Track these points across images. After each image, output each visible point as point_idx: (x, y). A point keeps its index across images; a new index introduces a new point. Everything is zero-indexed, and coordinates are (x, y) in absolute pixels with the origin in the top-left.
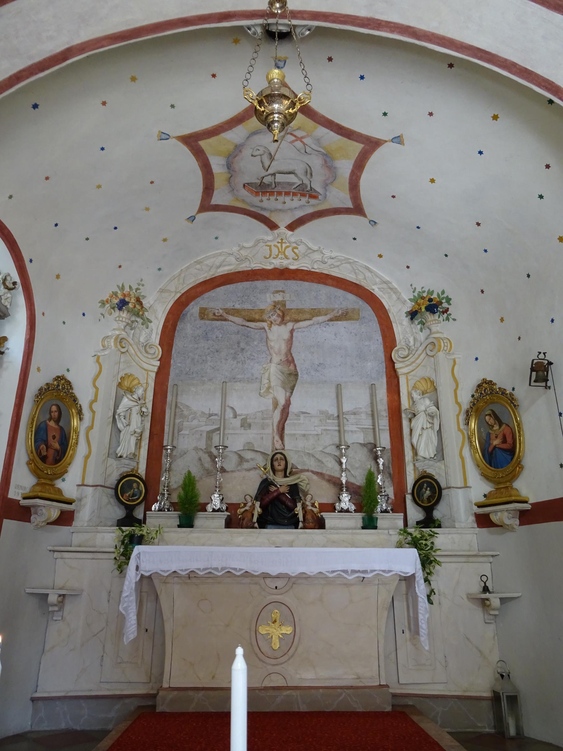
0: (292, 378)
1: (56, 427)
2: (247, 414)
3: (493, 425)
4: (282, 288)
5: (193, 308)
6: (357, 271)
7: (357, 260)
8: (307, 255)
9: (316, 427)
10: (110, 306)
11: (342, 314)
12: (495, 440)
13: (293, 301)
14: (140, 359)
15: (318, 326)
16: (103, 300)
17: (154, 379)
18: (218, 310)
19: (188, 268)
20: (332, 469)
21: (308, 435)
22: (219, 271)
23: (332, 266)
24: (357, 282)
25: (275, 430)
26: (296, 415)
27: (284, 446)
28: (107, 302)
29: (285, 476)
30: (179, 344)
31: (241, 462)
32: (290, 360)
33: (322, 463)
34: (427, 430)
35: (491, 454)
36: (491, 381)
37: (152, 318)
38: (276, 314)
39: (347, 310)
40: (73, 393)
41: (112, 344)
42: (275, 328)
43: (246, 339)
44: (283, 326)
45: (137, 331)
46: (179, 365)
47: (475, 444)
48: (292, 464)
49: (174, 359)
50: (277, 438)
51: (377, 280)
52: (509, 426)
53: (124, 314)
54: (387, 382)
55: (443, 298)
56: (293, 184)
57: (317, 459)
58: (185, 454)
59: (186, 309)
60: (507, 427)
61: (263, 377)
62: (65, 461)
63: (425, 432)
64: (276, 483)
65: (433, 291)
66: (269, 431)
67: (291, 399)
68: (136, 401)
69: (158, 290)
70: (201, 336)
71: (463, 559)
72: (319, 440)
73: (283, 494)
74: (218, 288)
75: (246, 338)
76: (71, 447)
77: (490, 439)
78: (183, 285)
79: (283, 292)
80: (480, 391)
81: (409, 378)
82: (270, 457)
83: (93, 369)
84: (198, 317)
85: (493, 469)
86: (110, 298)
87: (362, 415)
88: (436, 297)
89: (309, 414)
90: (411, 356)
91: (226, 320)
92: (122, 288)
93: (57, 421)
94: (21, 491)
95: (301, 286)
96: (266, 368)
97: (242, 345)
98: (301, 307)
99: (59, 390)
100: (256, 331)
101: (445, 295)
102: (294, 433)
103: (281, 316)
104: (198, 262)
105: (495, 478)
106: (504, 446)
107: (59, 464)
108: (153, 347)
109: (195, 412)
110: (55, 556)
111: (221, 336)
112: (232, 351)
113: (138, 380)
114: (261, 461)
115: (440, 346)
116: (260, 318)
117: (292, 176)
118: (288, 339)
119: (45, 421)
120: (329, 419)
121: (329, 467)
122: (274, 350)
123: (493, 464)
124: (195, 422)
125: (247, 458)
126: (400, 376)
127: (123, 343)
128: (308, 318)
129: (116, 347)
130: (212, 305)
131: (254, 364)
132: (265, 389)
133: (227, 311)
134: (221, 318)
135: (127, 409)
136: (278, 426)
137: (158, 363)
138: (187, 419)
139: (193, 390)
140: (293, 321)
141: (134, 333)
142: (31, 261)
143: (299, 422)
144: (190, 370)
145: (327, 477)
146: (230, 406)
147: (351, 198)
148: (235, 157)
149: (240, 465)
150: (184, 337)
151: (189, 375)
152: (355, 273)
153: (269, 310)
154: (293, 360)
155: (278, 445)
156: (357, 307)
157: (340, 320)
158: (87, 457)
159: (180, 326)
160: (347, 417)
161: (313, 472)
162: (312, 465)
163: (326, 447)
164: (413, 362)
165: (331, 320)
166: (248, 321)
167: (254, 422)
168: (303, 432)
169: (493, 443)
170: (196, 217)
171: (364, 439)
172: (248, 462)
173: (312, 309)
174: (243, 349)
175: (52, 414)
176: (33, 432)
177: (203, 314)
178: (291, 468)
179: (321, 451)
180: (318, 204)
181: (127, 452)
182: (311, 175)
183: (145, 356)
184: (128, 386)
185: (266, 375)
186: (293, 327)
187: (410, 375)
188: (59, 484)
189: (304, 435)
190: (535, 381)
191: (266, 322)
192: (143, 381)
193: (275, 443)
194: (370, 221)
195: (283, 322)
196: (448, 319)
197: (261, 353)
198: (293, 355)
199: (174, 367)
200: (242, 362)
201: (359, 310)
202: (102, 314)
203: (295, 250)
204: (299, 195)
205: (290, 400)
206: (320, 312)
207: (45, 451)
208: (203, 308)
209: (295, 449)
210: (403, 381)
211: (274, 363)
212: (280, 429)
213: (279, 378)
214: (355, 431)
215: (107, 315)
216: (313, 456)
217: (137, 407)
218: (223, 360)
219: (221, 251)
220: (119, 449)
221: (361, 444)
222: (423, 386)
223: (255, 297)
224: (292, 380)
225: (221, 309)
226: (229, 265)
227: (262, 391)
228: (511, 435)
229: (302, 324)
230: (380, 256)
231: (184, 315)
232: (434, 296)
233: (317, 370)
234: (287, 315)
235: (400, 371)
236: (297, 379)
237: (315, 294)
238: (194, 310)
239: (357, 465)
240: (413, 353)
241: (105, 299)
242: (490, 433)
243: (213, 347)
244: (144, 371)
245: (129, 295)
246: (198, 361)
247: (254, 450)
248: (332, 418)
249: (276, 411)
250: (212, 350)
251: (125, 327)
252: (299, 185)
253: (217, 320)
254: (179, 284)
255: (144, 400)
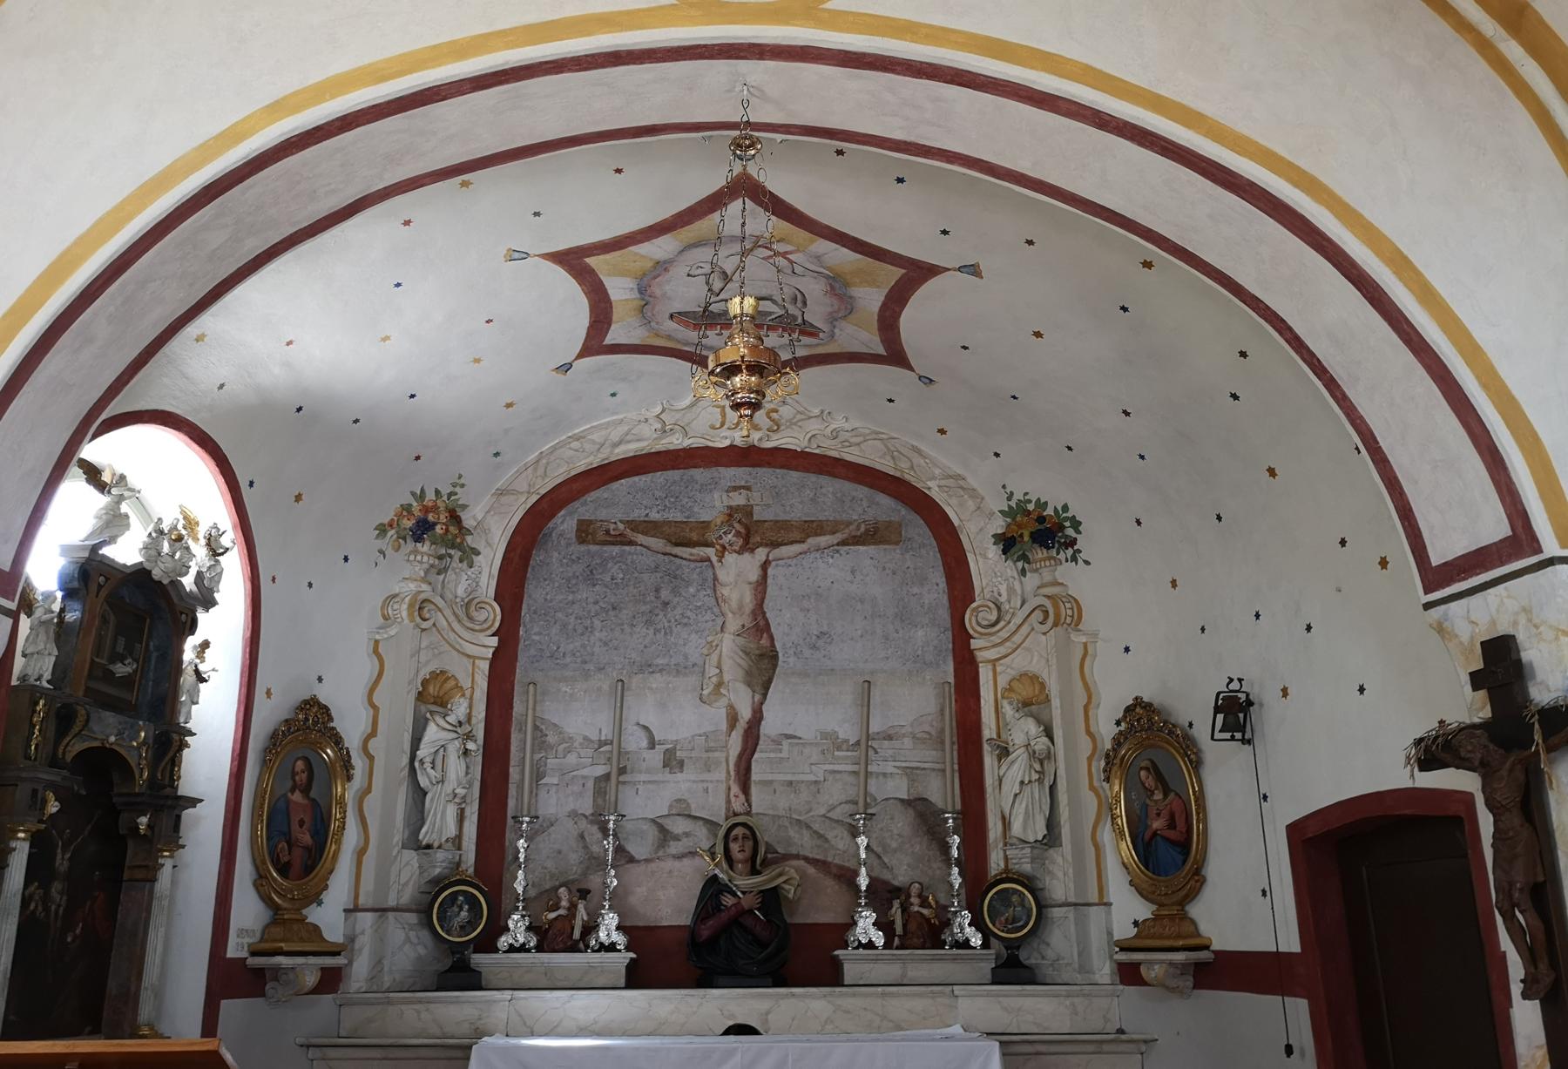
0: (765, 664)
1: (306, 802)
2: (676, 741)
3: (1153, 789)
4: (746, 482)
5: (562, 523)
6: (895, 453)
7: (896, 436)
8: (795, 424)
9: (813, 767)
10: (397, 532)
11: (867, 531)
12: (1156, 820)
13: (768, 506)
14: (460, 637)
15: (818, 555)
16: (382, 524)
17: (487, 673)
18: (615, 523)
19: (554, 448)
20: (844, 852)
21: (798, 782)
22: (617, 451)
23: (847, 444)
24: (898, 474)
25: (732, 773)
26: (773, 741)
27: (750, 806)
28: (391, 526)
29: (754, 872)
30: (536, 594)
31: (665, 840)
32: (760, 625)
33: (827, 840)
34: (1029, 785)
35: (1149, 844)
36: (1150, 705)
37: (480, 546)
38: (734, 531)
39: (876, 523)
40: (334, 728)
41: (404, 614)
42: (730, 558)
43: (672, 582)
44: (747, 555)
45: (450, 575)
46: (536, 638)
47: (1120, 822)
48: (767, 843)
49: (525, 626)
50: (735, 789)
51: (937, 472)
52: (1180, 797)
53: (425, 546)
54: (955, 671)
55: (1066, 519)
56: (771, 313)
57: (816, 832)
58: (552, 825)
59: (550, 525)
60: (1177, 798)
61: (707, 662)
62: (323, 866)
63: (1027, 789)
64: (734, 889)
65: (1046, 503)
66: (720, 774)
67: (764, 708)
68: (454, 729)
69: (494, 491)
70: (580, 578)
71: (1091, 1048)
72: (819, 792)
73: (751, 911)
74: (614, 483)
75: (673, 580)
76: (333, 837)
77: (1147, 816)
78: (543, 479)
79: (748, 488)
80: (1130, 720)
81: (999, 669)
82: (722, 833)
83: (365, 668)
84: (574, 540)
85: (1150, 874)
86: (396, 518)
87: (906, 740)
88: (1053, 514)
89: (800, 738)
90: (1002, 624)
91: (631, 543)
92: (420, 497)
93: (306, 791)
94: (247, 940)
95: (783, 478)
96: (714, 644)
97: (665, 594)
98: (782, 517)
99: (308, 728)
100: (693, 565)
101: (1069, 515)
102: (770, 778)
103: (744, 536)
104: (577, 438)
105: (1154, 893)
106: (1172, 834)
107: (311, 876)
108: (483, 605)
109: (571, 738)
110: (310, 1056)
111: (621, 576)
112: (643, 608)
113: (456, 679)
114: (702, 838)
115: (1057, 615)
116: (701, 539)
117: (768, 303)
118: (757, 581)
119: (285, 795)
120: (839, 748)
121: (839, 850)
122: (729, 605)
123: (1151, 866)
124: (572, 759)
125: (676, 832)
126: (980, 665)
127: (426, 610)
128: (798, 539)
129: (412, 620)
130: (602, 514)
131: (689, 634)
132: (712, 687)
133: (634, 526)
134: (621, 540)
135: (437, 748)
136: (738, 765)
137: (494, 642)
138: (554, 751)
139: (566, 692)
140: (767, 545)
141: (443, 581)
142: (251, 484)
143: (781, 755)
144: (558, 648)
145: (834, 870)
146: (641, 723)
147: (882, 341)
148: (655, 278)
149: (663, 847)
150: (545, 580)
151: (557, 659)
152: (893, 458)
153: (719, 523)
154: (768, 625)
155: (738, 805)
156: (895, 518)
157: (863, 544)
158: (361, 853)
159: (537, 557)
160: (875, 744)
161: (806, 859)
162: (804, 843)
163: (833, 808)
164: (1007, 640)
165: (843, 543)
166: (677, 545)
167: (691, 758)
168: (789, 777)
169: (1151, 826)
170: (574, 364)
171: (909, 791)
172: (680, 840)
173: (806, 522)
174: (666, 604)
175: (297, 778)
176: (265, 821)
177: (585, 532)
178: (765, 853)
179: (824, 816)
180: (817, 345)
181: (440, 839)
182: (805, 303)
183: (468, 628)
184: (436, 694)
185: (714, 657)
186: (768, 556)
187: (1001, 665)
188: (315, 915)
189: (790, 783)
190: (1220, 731)
191: (714, 547)
192: (466, 683)
193: (733, 799)
194: (920, 377)
195: (747, 547)
196: (1074, 559)
197: (704, 613)
198: (768, 615)
199: (526, 643)
200: (665, 632)
201: (900, 525)
202: (381, 552)
203: (774, 415)
204: (781, 329)
205: (761, 709)
206: (822, 528)
207: (287, 853)
208: (584, 520)
209: (771, 812)
210: (985, 674)
211: (730, 634)
212: (742, 772)
213: (739, 665)
214: (891, 774)
215: (390, 552)
216: (808, 827)
217: (456, 742)
218: (626, 626)
219: (621, 416)
220: (424, 830)
221: (902, 801)
222: (1026, 691)
223: (689, 498)
224: (765, 669)
225: (621, 521)
226: (638, 440)
227: (705, 692)
228: (1184, 816)
229: (785, 551)
230: (942, 431)
231: (545, 535)
232: (1049, 511)
233: (814, 647)
234: (756, 532)
235: (980, 655)
236: (775, 666)
237: (813, 494)
238: (565, 525)
239: (894, 845)
240: (1007, 618)
241: (386, 521)
242: (1147, 805)
243: (606, 599)
244: (465, 659)
245: (435, 509)
246: (575, 630)
247: (689, 816)
248: (844, 747)
249: (734, 733)
250: (604, 606)
251: (427, 572)
252: (779, 317)
253: (614, 544)
254: (537, 477)
255: (470, 725)
